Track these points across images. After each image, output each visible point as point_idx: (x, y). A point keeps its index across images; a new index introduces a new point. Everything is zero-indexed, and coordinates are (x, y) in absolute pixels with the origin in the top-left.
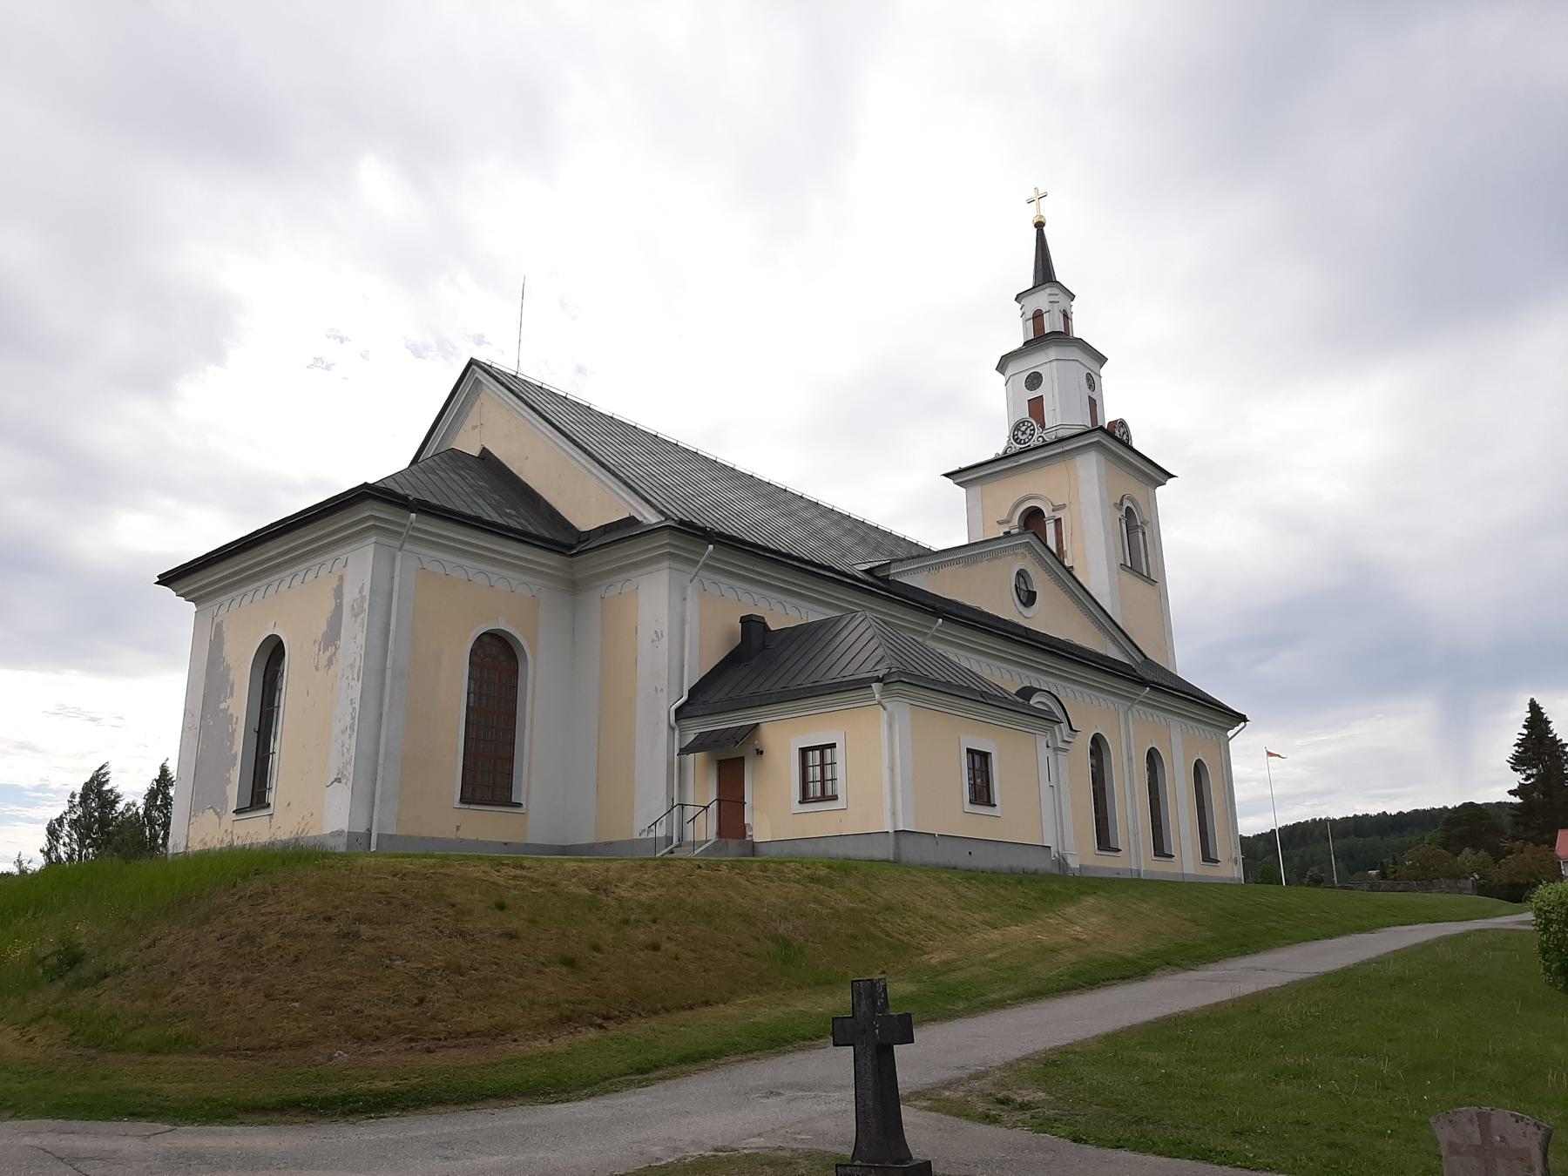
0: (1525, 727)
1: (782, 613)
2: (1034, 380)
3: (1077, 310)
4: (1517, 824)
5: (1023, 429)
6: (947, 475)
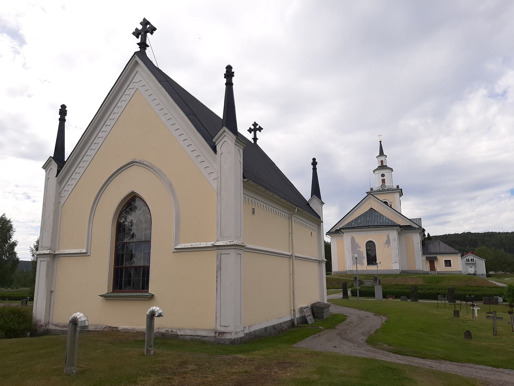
2: (383, 175)
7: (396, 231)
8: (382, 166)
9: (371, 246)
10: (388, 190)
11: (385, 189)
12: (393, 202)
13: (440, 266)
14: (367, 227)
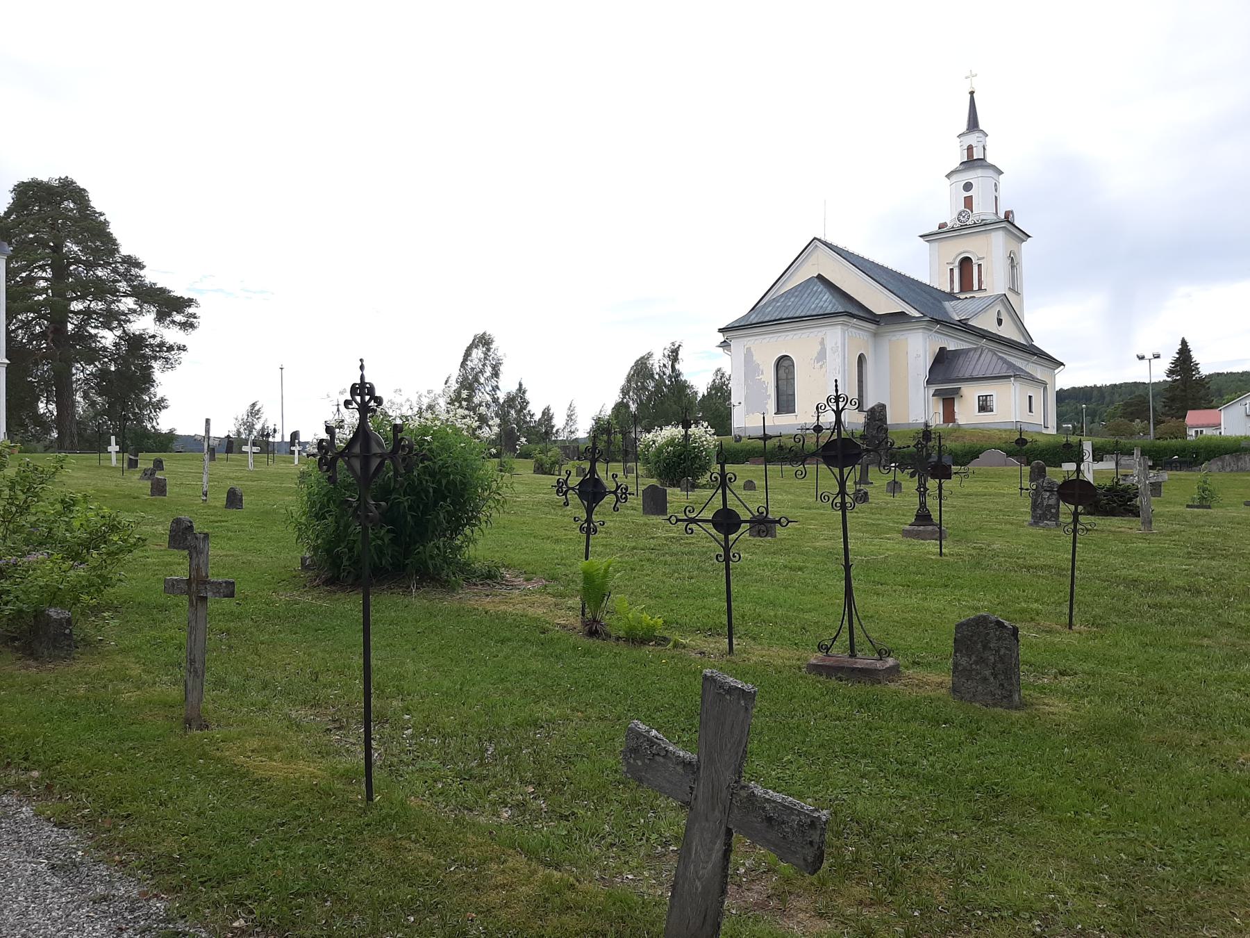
0: (1177, 353)
1: (952, 345)
2: (968, 187)
3: (989, 142)
4: (1166, 406)
5: (963, 215)
6: (921, 236)
7: (839, 327)
8: (972, 162)
9: (784, 365)
10: (975, 225)
11: (968, 223)
12: (985, 256)
13: (967, 413)
14: (760, 325)
